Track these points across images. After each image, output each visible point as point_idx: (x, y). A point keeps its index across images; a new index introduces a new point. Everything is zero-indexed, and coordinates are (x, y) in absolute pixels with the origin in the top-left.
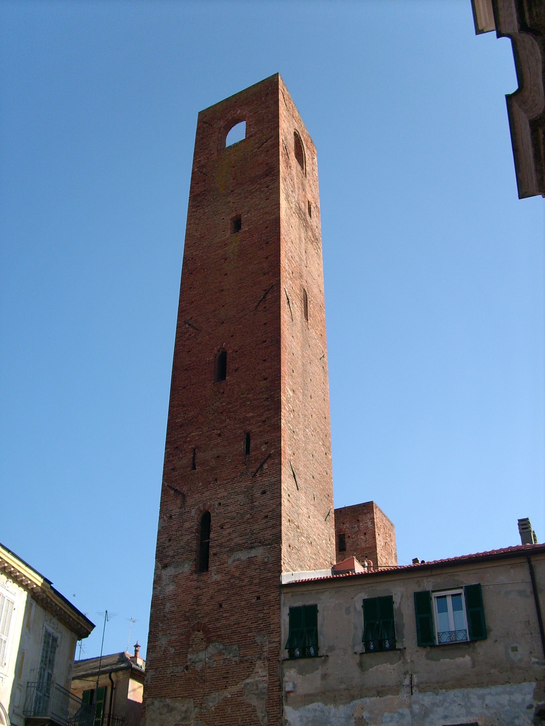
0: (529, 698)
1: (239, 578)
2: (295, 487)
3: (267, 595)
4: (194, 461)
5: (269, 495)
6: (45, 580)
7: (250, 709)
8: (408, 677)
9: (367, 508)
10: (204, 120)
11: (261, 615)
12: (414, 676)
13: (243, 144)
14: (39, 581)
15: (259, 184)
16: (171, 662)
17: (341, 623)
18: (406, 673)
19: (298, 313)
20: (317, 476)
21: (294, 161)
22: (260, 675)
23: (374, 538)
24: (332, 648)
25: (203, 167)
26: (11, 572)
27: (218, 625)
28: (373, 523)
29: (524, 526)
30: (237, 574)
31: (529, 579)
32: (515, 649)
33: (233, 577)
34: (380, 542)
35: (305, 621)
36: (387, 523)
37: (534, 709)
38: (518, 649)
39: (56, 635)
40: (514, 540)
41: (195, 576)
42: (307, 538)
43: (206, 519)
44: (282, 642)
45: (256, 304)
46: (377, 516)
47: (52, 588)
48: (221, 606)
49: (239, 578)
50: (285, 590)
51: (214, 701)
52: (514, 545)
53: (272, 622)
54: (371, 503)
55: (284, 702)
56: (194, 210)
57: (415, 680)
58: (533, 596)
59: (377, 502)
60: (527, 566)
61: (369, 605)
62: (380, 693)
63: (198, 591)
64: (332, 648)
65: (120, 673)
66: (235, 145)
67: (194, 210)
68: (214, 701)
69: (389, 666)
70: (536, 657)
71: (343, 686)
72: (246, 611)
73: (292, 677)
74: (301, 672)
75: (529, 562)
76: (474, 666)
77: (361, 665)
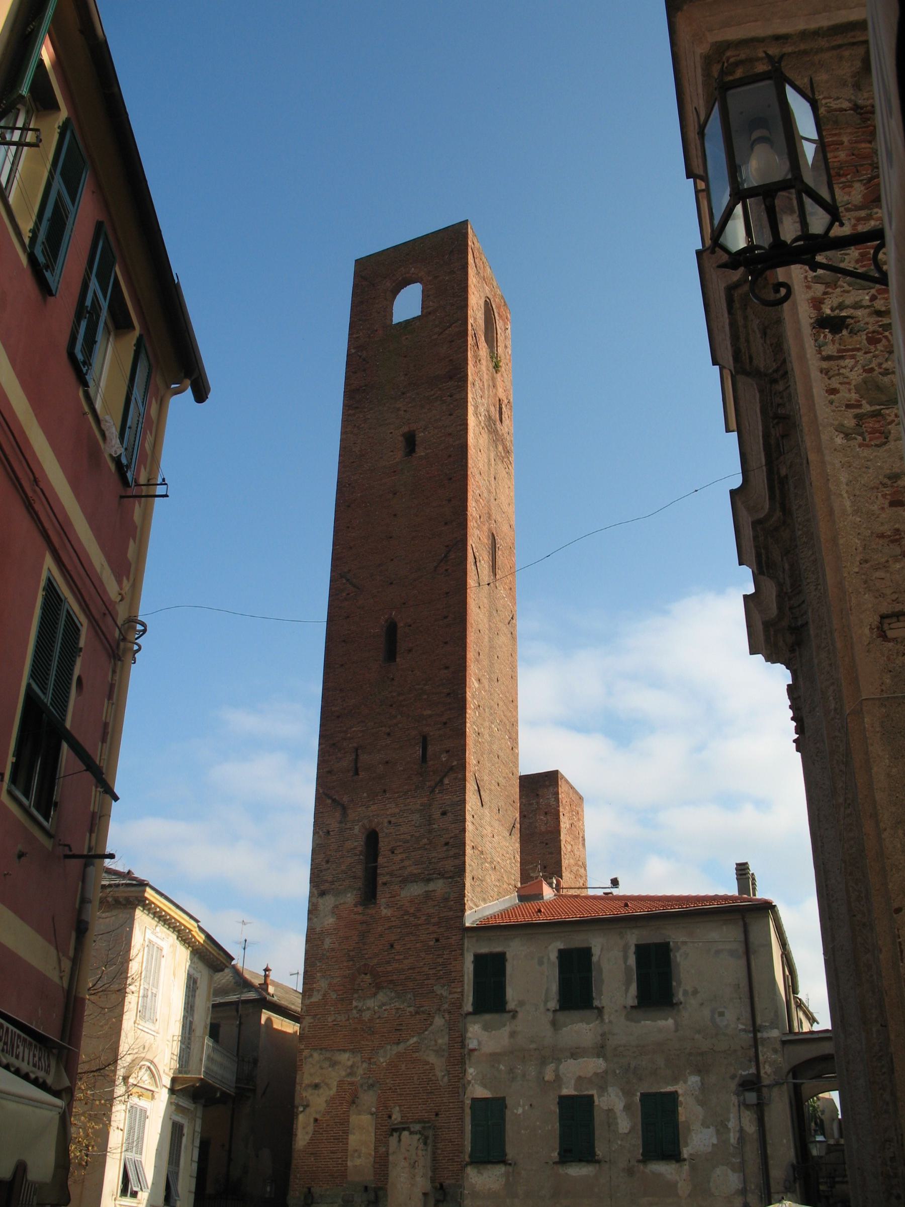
1: (414, 915)
5: (450, 817)
11: (440, 960)
15: (440, 389)
17: (531, 976)
21: (483, 344)
28: (557, 799)
29: (742, 870)
33: (407, 913)
37: (737, 1080)
40: (730, 888)
42: (491, 862)
48: (392, 946)
55: (467, 1062)
60: (741, 923)
66: (407, 322)
69: (584, 1026)
70: (742, 1024)
71: (533, 1046)
72: (423, 955)
73: (479, 1035)
76: (676, 1030)
77: (554, 1023)
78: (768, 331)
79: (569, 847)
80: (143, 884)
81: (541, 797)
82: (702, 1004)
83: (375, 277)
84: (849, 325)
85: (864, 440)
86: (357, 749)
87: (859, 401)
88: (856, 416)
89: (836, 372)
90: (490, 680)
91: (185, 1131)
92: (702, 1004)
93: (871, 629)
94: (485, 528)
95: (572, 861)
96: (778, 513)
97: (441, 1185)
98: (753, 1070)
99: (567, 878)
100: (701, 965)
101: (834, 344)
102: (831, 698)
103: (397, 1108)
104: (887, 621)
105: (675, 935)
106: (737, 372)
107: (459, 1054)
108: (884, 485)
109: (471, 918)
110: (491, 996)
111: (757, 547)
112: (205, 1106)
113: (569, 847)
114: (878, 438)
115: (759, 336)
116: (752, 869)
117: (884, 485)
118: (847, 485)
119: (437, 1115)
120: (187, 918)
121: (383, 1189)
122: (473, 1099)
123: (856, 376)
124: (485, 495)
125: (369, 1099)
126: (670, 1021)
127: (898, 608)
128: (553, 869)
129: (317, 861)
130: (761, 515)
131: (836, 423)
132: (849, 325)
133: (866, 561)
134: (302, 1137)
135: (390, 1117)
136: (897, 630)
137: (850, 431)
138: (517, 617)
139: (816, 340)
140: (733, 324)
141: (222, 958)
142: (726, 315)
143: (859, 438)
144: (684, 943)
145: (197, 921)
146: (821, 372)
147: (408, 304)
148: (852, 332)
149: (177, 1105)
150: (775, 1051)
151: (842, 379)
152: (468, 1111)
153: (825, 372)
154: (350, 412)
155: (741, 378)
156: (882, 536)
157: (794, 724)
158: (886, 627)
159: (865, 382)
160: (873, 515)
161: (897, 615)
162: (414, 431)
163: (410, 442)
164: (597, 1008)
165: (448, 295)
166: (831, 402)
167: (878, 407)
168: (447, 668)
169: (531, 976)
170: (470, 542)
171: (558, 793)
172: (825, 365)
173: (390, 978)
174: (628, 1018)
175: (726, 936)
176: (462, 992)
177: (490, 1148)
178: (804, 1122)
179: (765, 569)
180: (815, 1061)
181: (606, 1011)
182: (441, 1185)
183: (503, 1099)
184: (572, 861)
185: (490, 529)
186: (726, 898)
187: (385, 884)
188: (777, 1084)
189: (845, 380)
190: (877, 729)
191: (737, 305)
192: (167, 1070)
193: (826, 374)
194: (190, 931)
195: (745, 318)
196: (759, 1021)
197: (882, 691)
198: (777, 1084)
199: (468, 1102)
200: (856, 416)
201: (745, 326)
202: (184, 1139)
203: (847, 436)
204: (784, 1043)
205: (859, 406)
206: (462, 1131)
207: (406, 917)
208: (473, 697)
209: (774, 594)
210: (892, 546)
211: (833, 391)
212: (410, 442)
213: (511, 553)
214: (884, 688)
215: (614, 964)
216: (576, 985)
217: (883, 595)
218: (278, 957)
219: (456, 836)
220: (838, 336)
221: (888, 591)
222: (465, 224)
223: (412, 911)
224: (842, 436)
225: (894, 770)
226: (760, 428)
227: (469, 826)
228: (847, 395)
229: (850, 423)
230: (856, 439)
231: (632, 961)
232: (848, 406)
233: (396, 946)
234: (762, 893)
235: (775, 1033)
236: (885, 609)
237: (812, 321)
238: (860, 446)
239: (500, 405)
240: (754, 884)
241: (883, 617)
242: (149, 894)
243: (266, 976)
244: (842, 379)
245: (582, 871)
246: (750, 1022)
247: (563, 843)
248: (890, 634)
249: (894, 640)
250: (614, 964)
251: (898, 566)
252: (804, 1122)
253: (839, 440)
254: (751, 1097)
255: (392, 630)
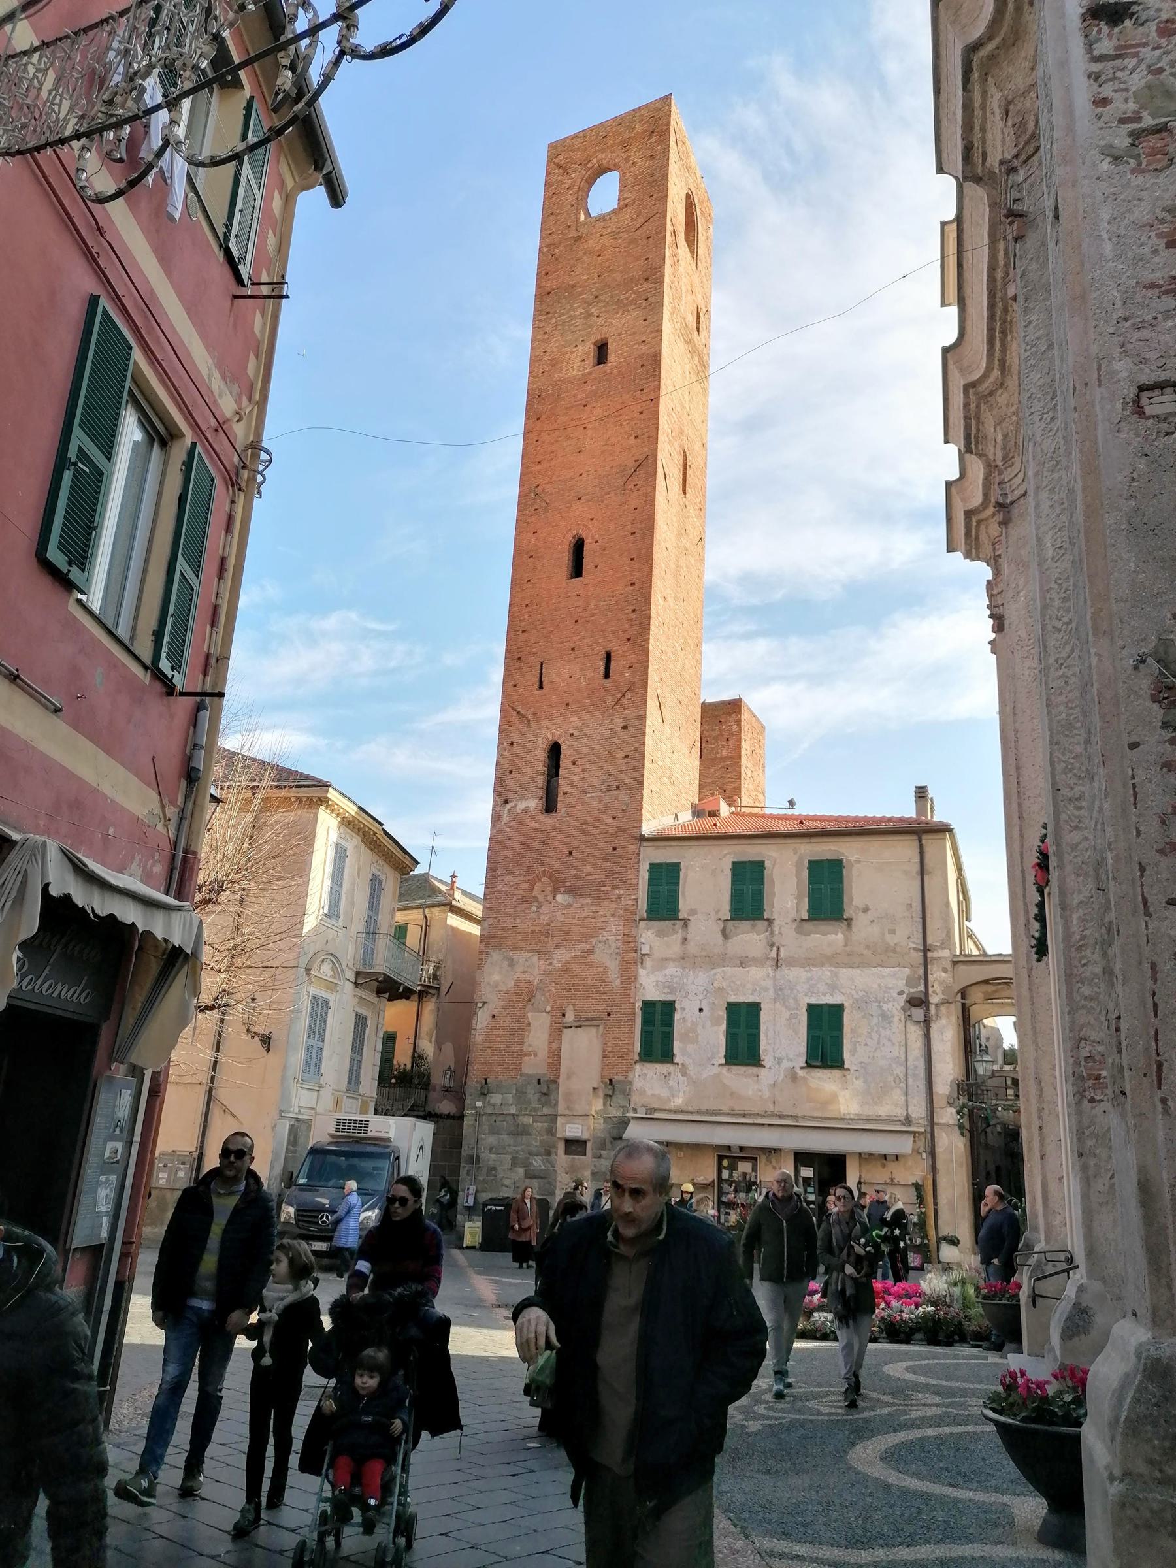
3: (625, 847)
5: (631, 732)
6: (361, 808)
7: (601, 969)
9: (734, 706)
10: (556, 160)
12: (782, 949)
13: (614, 219)
14: (352, 810)
15: (635, 292)
17: (705, 886)
19: (676, 487)
20: (685, 700)
21: (682, 243)
22: (612, 933)
23: (739, 746)
24: (693, 912)
25: (553, 245)
26: (359, 829)
28: (739, 727)
29: (921, 793)
30: (590, 819)
31: (917, 860)
32: (892, 932)
33: (586, 822)
34: (745, 748)
35: (666, 880)
36: (756, 725)
39: (382, 877)
40: (907, 809)
42: (670, 777)
43: (555, 751)
46: (745, 716)
48: (571, 853)
50: (645, 844)
51: (560, 957)
54: (740, 700)
57: (782, 954)
58: (919, 878)
59: (745, 699)
60: (916, 843)
61: (738, 869)
62: (742, 964)
64: (693, 912)
65: (436, 909)
68: (560, 957)
69: (755, 936)
71: (704, 953)
73: (649, 937)
74: (660, 934)
75: (920, 841)
76: (846, 945)
77: (725, 935)
78: (1011, 107)
79: (749, 773)
80: (325, 785)
81: (721, 723)
82: (872, 921)
83: (571, 165)
84: (1133, 14)
85: (1140, 164)
87: (1139, 113)
88: (1131, 134)
89: (1111, 76)
90: (676, 599)
91: (369, 1023)
92: (872, 921)
93: (1125, 404)
94: (676, 444)
95: (751, 786)
96: (996, 373)
97: (611, 1081)
98: (922, 988)
99: (745, 800)
100: (876, 880)
101: (1110, 39)
102: (1048, 545)
103: (571, 1007)
104: (1145, 395)
106: (965, 178)
107: (632, 957)
108: (1162, 221)
109: (649, 827)
110: (664, 902)
111: (967, 418)
113: (749, 773)
114: (1159, 161)
115: (998, 118)
116: (931, 794)
117: (1162, 221)
118: (1109, 223)
119: (609, 1015)
123: (1138, 81)
124: (678, 409)
126: (840, 936)
127: (1163, 376)
128: (732, 794)
130: (975, 376)
131: (1103, 143)
132: (1133, 14)
133: (1126, 319)
134: (478, 1038)
136: (1160, 404)
137: (1121, 153)
138: (707, 539)
139: (1086, 36)
140: (967, 107)
142: (960, 93)
143: (1132, 161)
144: (858, 862)
145: (381, 824)
146: (1089, 77)
147: (605, 196)
148: (1138, 24)
150: (945, 970)
151: (1117, 85)
152: (638, 1012)
153: (1095, 77)
154: (542, 317)
155: (970, 187)
156: (1152, 286)
157: (991, 621)
158: (1144, 401)
159: (1149, 87)
160: (1141, 260)
161: (1161, 386)
164: (768, 920)
165: (649, 187)
166: (1099, 117)
167: (1163, 120)
169: (705, 886)
170: (660, 457)
171: (740, 720)
172: (1096, 67)
175: (905, 849)
176: (636, 900)
178: (970, 1043)
179: (973, 446)
180: (985, 984)
181: (777, 923)
184: (751, 786)
185: (682, 446)
186: (902, 820)
188: (946, 1002)
189: (1122, 86)
190: (1123, 527)
191: (976, 75)
192: (350, 965)
193: (1096, 80)
194: (375, 833)
195: (984, 94)
196: (929, 941)
197: (1133, 479)
198: (946, 1002)
200: (1131, 134)
201: (983, 107)
202: (367, 1031)
203: (1116, 159)
204: (955, 963)
205: (1139, 119)
208: (658, 614)
209: (981, 476)
210: (1163, 298)
211: (1103, 102)
213: (704, 474)
214: (1135, 475)
216: (748, 895)
217: (1144, 361)
218: (456, 842)
219: (635, 750)
220: (1116, 30)
221: (1153, 356)
222: (667, 99)
224: (1109, 159)
225: (1142, 576)
226: (986, 259)
227: (649, 740)
228: (1123, 107)
229: (1121, 141)
230: (1127, 163)
232: (1122, 121)
234: (939, 816)
235: (946, 953)
236: (1147, 377)
237: (1084, 10)
238: (1133, 171)
239: (698, 312)
240: (932, 808)
241: (1142, 388)
242: (332, 794)
244: (1117, 85)
245: (761, 797)
246: (920, 941)
247: (743, 768)
248: (1149, 410)
249: (1156, 417)
251: (1169, 323)
252: (970, 1043)
253: (1105, 165)
254: (918, 1014)
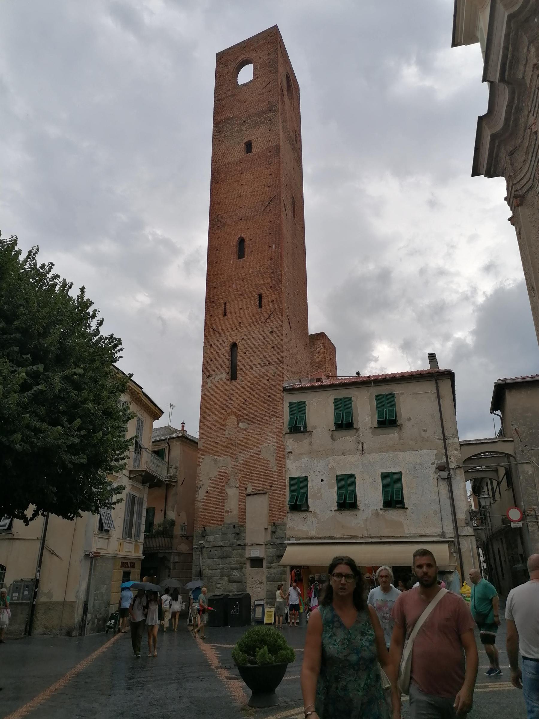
0: (432, 459)
1: (256, 384)
2: (289, 328)
3: (275, 395)
4: (225, 311)
8: (361, 444)
11: (271, 407)
12: (364, 444)
13: (252, 84)
15: (264, 118)
16: (245, 470)
18: (359, 443)
24: (315, 427)
27: (244, 412)
29: (432, 357)
32: (425, 431)
33: (253, 383)
37: (435, 465)
38: (260, 309)
40: (426, 366)
41: (229, 383)
42: (296, 360)
44: (285, 423)
45: (264, 208)
47: (142, 391)
48: (246, 400)
49: (256, 384)
52: (426, 369)
53: (278, 411)
55: (286, 458)
56: (217, 134)
60: (434, 382)
62: (343, 454)
63: (231, 392)
64: (315, 427)
66: (245, 85)
67: (217, 134)
70: (437, 436)
71: (321, 449)
72: (262, 404)
77: (332, 436)
83: (228, 62)
86: (225, 304)
98: (444, 460)
100: (413, 406)
103: (250, 484)
105: (398, 389)
107: (282, 455)
112: (150, 487)
120: (136, 386)
121: (243, 526)
122: (291, 478)
125: (234, 482)
129: (206, 361)
134: (200, 505)
135: (246, 489)
141: (157, 411)
149: (133, 486)
162: (251, 141)
163: (249, 146)
164: (355, 429)
168: (271, 259)
173: (245, 417)
174: (373, 433)
177: (299, 504)
182: (274, 523)
183: (306, 478)
187: (241, 369)
196: (446, 434)
198: (458, 468)
199: (287, 480)
206: (285, 495)
207: (252, 386)
212: (249, 146)
215: (365, 411)
223: (255, 382)
231: (374, 402)
233: (248, 401)
243: (183, 427)
250: (365, 411)
254: (444, 474)
255: (242, 241)
